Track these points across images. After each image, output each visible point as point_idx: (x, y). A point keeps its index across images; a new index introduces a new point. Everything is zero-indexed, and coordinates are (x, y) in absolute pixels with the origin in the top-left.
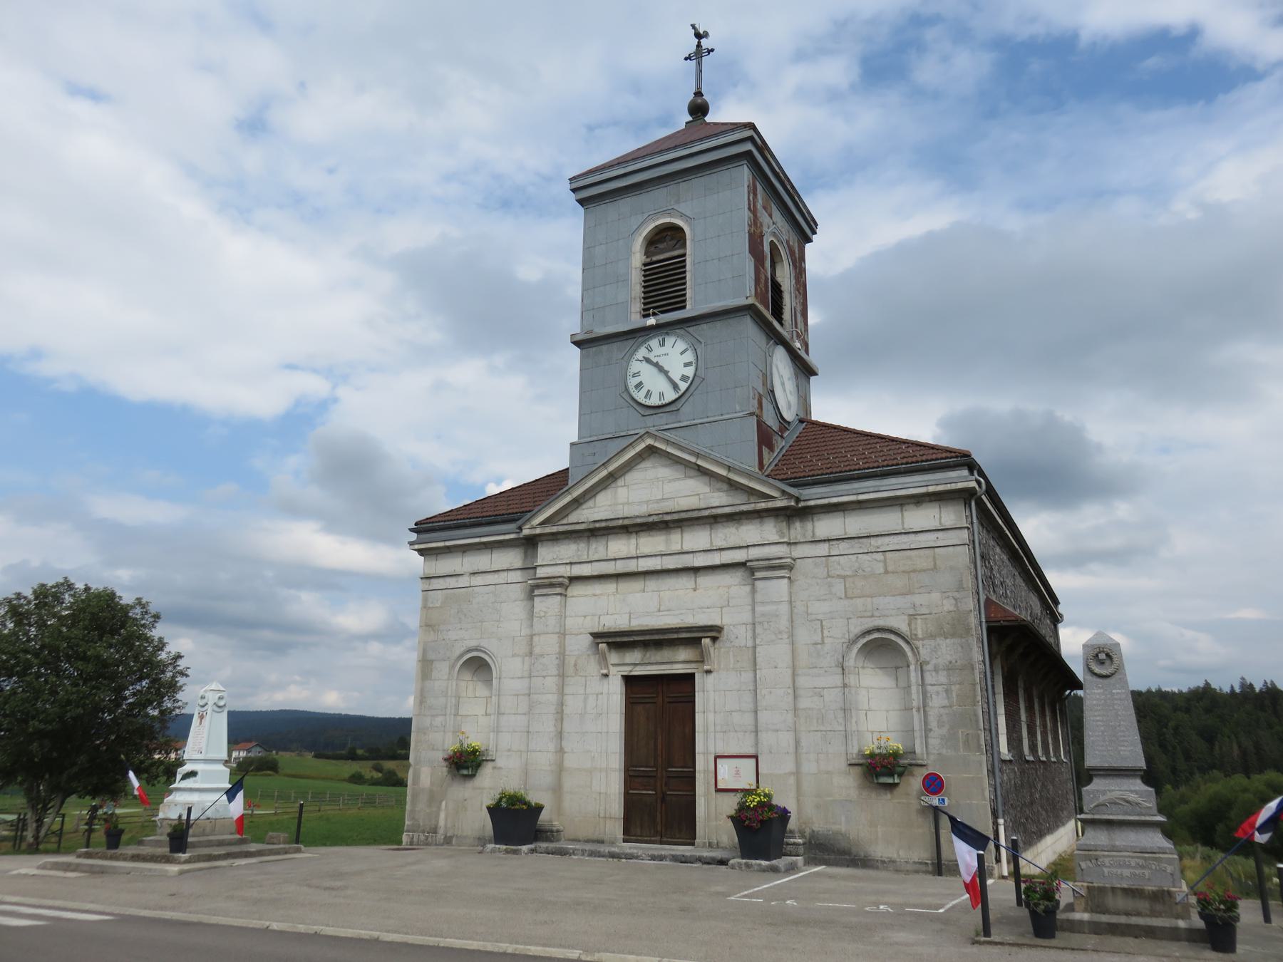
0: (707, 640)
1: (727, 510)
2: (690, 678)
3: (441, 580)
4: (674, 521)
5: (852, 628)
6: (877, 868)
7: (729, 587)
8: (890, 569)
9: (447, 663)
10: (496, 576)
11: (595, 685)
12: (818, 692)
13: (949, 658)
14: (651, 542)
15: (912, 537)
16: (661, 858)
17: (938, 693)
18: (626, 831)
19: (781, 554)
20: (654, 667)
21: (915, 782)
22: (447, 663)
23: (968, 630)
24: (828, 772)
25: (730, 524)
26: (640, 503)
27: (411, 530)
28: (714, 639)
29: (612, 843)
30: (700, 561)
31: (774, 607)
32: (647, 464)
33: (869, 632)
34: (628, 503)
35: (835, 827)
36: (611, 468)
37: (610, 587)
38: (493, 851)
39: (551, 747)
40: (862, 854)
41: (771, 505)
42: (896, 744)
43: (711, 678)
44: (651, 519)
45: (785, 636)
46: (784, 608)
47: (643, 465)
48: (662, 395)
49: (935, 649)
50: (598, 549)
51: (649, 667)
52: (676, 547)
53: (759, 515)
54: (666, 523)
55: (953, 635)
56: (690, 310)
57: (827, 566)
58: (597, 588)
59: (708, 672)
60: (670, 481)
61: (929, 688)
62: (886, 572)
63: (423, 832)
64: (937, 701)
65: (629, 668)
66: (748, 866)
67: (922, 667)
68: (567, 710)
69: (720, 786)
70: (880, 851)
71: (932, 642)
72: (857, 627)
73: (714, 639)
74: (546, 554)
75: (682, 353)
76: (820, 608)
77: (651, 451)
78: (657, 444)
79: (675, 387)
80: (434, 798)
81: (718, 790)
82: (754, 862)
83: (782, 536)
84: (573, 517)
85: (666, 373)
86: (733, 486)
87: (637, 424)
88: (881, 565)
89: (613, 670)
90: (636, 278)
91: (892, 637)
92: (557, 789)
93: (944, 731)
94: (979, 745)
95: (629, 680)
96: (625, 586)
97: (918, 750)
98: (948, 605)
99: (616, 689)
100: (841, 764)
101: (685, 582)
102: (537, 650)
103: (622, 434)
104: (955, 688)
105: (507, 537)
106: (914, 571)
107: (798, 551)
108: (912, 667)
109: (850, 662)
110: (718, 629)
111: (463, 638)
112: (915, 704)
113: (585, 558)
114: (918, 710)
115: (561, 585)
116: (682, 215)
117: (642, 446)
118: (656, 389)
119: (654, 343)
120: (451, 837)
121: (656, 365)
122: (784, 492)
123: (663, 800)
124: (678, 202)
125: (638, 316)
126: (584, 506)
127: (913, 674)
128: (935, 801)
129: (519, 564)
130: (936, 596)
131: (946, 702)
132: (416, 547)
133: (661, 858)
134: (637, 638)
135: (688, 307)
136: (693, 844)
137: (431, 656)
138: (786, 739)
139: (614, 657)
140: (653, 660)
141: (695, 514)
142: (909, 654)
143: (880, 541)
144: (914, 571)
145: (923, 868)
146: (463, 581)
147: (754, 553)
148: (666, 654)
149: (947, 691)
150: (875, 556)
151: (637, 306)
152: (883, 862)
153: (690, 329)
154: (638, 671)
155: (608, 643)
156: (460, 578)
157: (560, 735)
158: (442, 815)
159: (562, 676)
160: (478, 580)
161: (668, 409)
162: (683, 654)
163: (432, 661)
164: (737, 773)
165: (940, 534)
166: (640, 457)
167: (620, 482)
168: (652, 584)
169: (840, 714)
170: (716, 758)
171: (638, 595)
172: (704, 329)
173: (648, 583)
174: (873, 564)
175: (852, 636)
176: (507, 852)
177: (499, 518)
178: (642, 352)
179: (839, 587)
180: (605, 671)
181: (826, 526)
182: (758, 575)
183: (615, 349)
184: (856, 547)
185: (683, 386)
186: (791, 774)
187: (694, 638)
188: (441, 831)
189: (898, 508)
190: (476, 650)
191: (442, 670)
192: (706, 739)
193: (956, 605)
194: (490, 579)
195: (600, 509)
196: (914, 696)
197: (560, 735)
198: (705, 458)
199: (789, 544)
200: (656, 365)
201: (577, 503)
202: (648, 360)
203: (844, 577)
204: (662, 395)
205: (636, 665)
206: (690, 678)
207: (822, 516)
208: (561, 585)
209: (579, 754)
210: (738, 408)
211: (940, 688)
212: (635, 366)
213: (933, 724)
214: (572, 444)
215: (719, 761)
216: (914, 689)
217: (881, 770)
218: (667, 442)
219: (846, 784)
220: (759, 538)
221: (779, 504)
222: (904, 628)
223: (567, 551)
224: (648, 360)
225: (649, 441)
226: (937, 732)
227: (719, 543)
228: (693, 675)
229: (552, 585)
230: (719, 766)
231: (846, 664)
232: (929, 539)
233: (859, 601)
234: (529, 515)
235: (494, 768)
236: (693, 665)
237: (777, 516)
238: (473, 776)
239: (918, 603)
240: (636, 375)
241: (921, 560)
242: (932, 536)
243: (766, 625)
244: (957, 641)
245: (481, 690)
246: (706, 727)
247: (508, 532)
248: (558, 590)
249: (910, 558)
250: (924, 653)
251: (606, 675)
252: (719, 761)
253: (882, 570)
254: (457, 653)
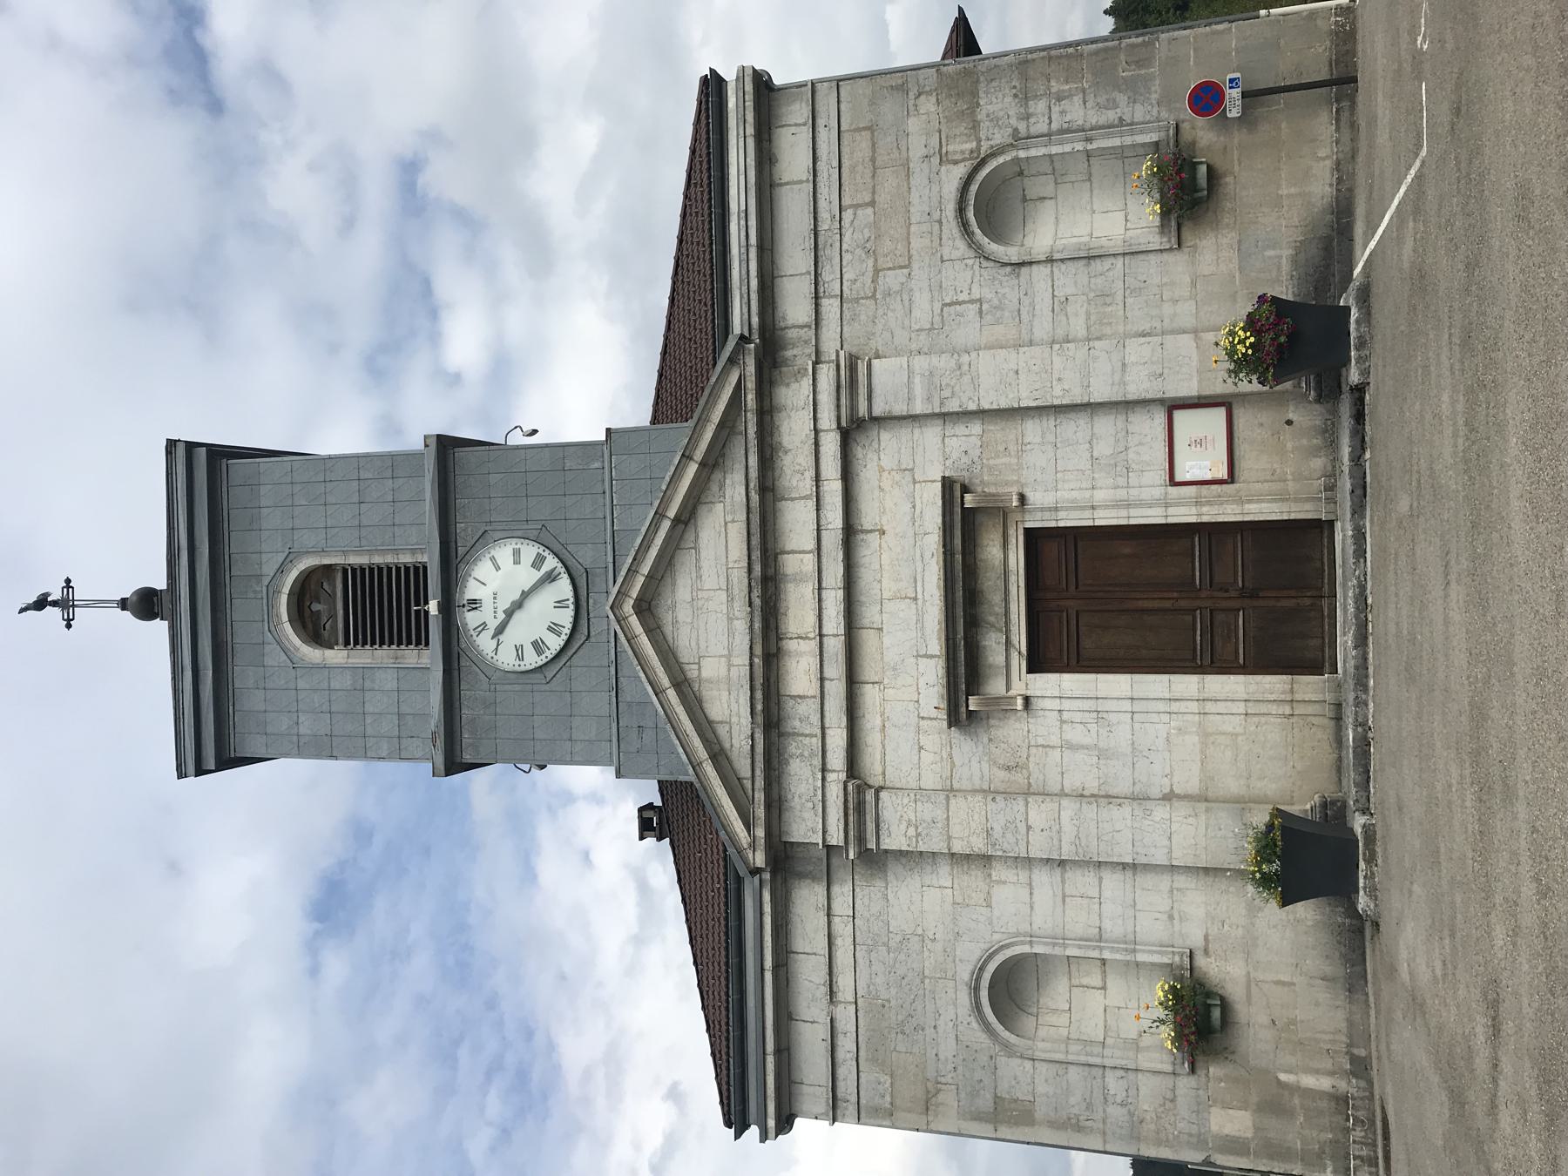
0: (968, 497)
1: (753, 461)
2: (1033, 538)
3: (841, 1072)
4: (764, 566)
5: (956, 254)
6: (1351, 190)
7: (881, 470)
8: (868, 199)
9: (1002, 1060)
10: (839, 942)
11: (1044, 727)
12: (1060, 305)
13: (1008, 99)
14: (799, 613)
15: (821, 165)
16: (1359, 536)
17: (1063, 112)
18: (1315, 668)
19: (833, 373)
20: (1013, 607)
21: (1202, 132)
22: (1002, 1060)
23: (967, 73)
24: (1193, 284)
25: (778, 464)
26: (731, 633)
27: (738, 1136)
28: (965, 489)
29: (1339, 686)
30: (834, 517)
31: (917, 380)
32: (667, 619)
33: (964, 225)
34: (729, 657)
35: (1286, 266)
36: (665, 681)
37: (870, 696)
38: (1373, 892)
39: (1160, 812)
40: (1328, 217)
41: (751, 384)
42: (1159, 990)
43: (1035, 498)
44: (757, 602)
45: (965, 358)
46: (920, 363)
47: (668, 630)
48: (560, 604)
49: (995, 120)
50: (801, 716)
51: (1014, 617)
52: (809, 562)
53: (767, 413)
54: (767, 679)
55: (975, 94)
56: (430, 558)
57: (857, 300)
58: (871, 721)
59: (1022, 498)
60: (700, 577)
61: (1055, 126)
62: (872, 203)
63: (1347, 1130)
64: (1076, 112)
65: (1015, 655)
66: (1362, 344)
67: (1018, 139)
68: (1092, 786)
69: (1223, 473)
70: (1321, 188)
71: (985, 125)
72: (956, 246)
73: (965, 489)
74: (804, 827)
75: (498, 568)
76: (924, 309)
77: (646, 608)
78: (634, 593)
79: (550, 577)
80: (1275, 1102)
81: (1232, 478)
82: (1353, 334)
83: (801, 372)
84: (743, 766)
85: (525, 595)
86: (713, 463)
87: (594, 657)
88: (860, 212)
89: (1018, 688)
90: (364, 656)
91: (974, 188)
92: (1241, 803)
93: (1122, 99)
94: (1144, 44)
95: (1036, 665)
96: (869, 669)
97: (1154, 137)
98: (928, 105)
99: (1046, 684)
100: (1178, 263)
101: (871, 552)
102: (978, 845)
103: (613, 689)
104: (1055, 86)
105: (767, 908)
106: (873, 160)
107: (830, 345)
108: (1022, 154)
109: (1012, 253)
110: (947, 484)
111: (953, 1015)
112: (1079, 146)
113: (816, 742)
114: (1089, 140)
115: (860, 790)
116: (281, 570)
117: (634, 621)
118: (546, 618)
119: (471, 619)
120: (1354, 1060)
121: (509, 614)
122: (732, 361)
123: (1253, 595)
124: (259, 577)
125: (426, 653)
126: (727, 745)
127: (1033, 152)
128: (1233, 95)
129: (820, 890)
130: (913, 124)
131: (1077, 99)
132: (772, 1132)
133: (1359, 536)
134: (961, 634)
135: (425, 559)
136: (1331, 523)
137: (985, 1102)
138: (1137, 351)
139: (996, 687)
140: (1000, 610)
141: (756, 519)
142: (1001, 160)
143: (824, 215)
144: (873, 160)
145: (1345, 115)
146: (845, 1016)
147: (827, 420)
148: (989, 583)
149: (1059, 100)
150: (846, 223)
151: (411, 656)
152: (1340, 181)
153: (461, 551)
154: (1020, 638)
155: (968, 695)
156: (840, 1026)
157: (1139, 798)
158: (1309, 1081)
159: (1027, 793)
160: (845, 983)
161: (583, 592)
162: (991, 550)
163: (997, 1099)
164: (1200, 443)
165: (820, 122)
166: (654, 631)
167: (692, 672)
168: (869, 614)
169: (1097, 266)
170: (1173, 483)
171: (887, 641)
172: (464, 530)
173: (866, 622)
174: (858, 225)
175: (972, 254)
176: (1371, 860)
177: (733, 960)
178: (485, 643)
179: (892, 279)
180: (1020, 701)
181: (795, 307)
182: (862, 410)
183: (471, 694)
184: (830, 254)
185: (551, 562)
186: (1197, 338)
187: (965, 518)
188: (1343, 1086)
189: (777, 281)
190: (976, 990)
191: (1016, 1076)
192: (1141, 504)
193: (929, 93)
194: (843, 956)
195: (731, 708)
196: (1067, 148)
197: (1139, 798)
198: (665, 501)
199: (816, 363)
200: (509, 614)
201: (719, 756)
202: (500, 630)
203: (877, 271)
204: (560, 604)
205: (1008, 643)
206: (1033, 538)
207: (779, 314)
208: (860, 790)
209: (1177, 750)
210: (597, 465)
211: (1055, 109)
212: (506, 659)
213: (1112, 116)
214: (619, 775)
215: (1178, 478)
216: (1055, 150)
217: (1187, 193)
218: (632, 571)
219: (1213, 252)
220: (805, 413)
221: (751, 369)
222: (960, 171)
223: (801, 778)
224: (500, 630)
225: (628, 607)
226: (1124, 108)
227: (806, 485)
228: (1029, 532)
229: (860, 808)
230: (1188, 478)
231: (1015, 260)
232: (827, 139)
233: (916, 243)
234: (731, 851)
235: (1206, 952)
236: (1012, 532)
237: (772, 383)
238: (1225, 1005)
239: (924, 151)
240: (519, 651)
241: (858, 149)
242: (823, 135)
243: (947, 393)
244: (982, 87)
245: (1057, 994)
246: (1117, 505)
247: (757, 903)
248: (870, 796)
249: (853, 168)
250: (1000, 137)
251: (1027, 699)
252: (1178, 478)
253: (870, 210)
254: (982, 1037)
